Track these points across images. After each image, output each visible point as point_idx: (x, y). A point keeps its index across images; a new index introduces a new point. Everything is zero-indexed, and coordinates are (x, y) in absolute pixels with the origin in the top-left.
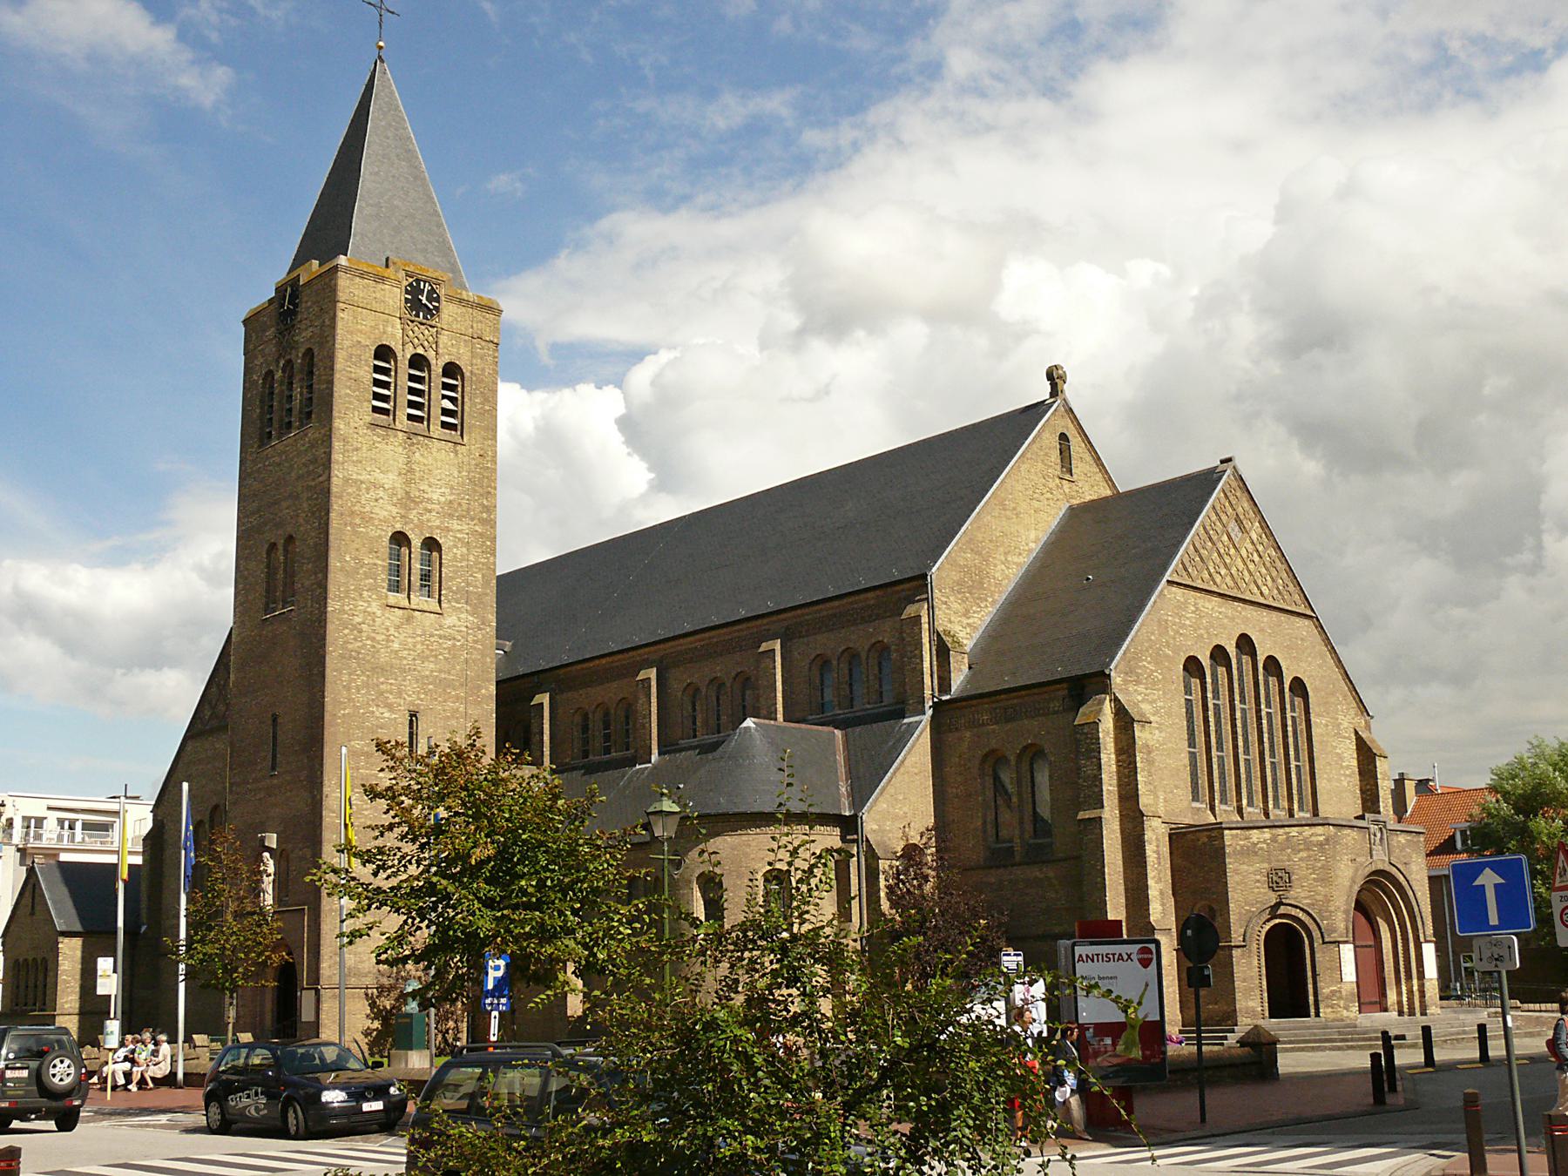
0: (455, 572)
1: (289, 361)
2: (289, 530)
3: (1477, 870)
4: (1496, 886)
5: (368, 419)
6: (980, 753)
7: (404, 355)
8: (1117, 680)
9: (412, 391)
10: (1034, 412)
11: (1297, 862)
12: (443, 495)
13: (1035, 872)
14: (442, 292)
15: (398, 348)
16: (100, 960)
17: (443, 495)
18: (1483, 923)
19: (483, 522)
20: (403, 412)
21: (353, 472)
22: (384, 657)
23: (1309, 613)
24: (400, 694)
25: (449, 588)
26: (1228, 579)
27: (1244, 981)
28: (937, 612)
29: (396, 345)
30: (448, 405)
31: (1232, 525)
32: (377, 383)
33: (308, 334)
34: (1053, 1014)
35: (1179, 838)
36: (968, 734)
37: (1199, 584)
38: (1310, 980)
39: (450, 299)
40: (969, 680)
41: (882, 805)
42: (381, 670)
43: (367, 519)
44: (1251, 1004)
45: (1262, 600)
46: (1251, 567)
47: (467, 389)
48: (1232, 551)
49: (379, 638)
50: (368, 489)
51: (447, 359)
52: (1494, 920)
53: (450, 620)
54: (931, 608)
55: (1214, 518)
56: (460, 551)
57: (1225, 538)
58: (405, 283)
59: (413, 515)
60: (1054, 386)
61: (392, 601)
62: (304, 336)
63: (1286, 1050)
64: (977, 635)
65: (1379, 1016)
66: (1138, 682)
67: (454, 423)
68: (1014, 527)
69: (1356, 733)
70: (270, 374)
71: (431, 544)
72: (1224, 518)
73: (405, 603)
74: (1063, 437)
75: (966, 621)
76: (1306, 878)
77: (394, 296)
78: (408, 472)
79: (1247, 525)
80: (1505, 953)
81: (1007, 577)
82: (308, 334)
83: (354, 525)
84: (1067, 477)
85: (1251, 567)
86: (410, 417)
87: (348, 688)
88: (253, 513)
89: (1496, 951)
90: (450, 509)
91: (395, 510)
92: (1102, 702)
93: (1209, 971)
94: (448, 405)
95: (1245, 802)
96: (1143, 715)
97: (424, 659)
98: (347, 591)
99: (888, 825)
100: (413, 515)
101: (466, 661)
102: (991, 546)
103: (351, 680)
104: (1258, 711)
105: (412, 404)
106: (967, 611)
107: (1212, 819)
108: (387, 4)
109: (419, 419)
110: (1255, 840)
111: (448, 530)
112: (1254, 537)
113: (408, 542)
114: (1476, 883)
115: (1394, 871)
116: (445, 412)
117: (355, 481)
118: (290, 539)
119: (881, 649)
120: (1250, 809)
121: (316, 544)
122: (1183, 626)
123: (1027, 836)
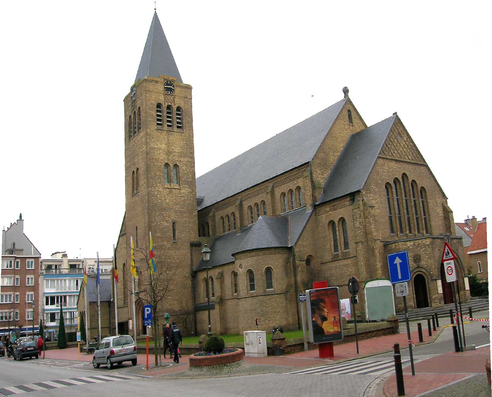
1: (135, 112)
2: (137, 166)
6: (328, 221)
7: (165, 106)
11: (422, 252)
13: (345, 262)
20: (166, 124)
32: (158, 115)
34: (353, 309)
37: (388, 157)
38: (428, 293)
44: (411, 303)
45: (409, 161)
46: (405, 150)
51: (177, 105)
52: (400, 277)
53: (183, 191)
55: (392, 134)
56: (184, 168)
57: (396, 140)
61: (166, 186)
63: (401, 322)
66: (371, 193)
69: (443, 204)
70: (130, 116)
71: (176, 166)
73: (169, 187)
74: (349, 111)
75: (322, 177)
76: (425, 258)
77: (161, 87)
78: (168, 144)
81: (334, 160)
83: (153, 162)
84: (351, 124)
85: (405, 150)
86: (168, 126)
87: (154, 216)
90: (181, 155)
93: (357, 298)
95: (408, 232)
102: (329, 150)
103: (155, 214)
105: (168, 121)
109: (160, 124)
110: (408, 245)
113: (399, 181)
116: (178, 123)
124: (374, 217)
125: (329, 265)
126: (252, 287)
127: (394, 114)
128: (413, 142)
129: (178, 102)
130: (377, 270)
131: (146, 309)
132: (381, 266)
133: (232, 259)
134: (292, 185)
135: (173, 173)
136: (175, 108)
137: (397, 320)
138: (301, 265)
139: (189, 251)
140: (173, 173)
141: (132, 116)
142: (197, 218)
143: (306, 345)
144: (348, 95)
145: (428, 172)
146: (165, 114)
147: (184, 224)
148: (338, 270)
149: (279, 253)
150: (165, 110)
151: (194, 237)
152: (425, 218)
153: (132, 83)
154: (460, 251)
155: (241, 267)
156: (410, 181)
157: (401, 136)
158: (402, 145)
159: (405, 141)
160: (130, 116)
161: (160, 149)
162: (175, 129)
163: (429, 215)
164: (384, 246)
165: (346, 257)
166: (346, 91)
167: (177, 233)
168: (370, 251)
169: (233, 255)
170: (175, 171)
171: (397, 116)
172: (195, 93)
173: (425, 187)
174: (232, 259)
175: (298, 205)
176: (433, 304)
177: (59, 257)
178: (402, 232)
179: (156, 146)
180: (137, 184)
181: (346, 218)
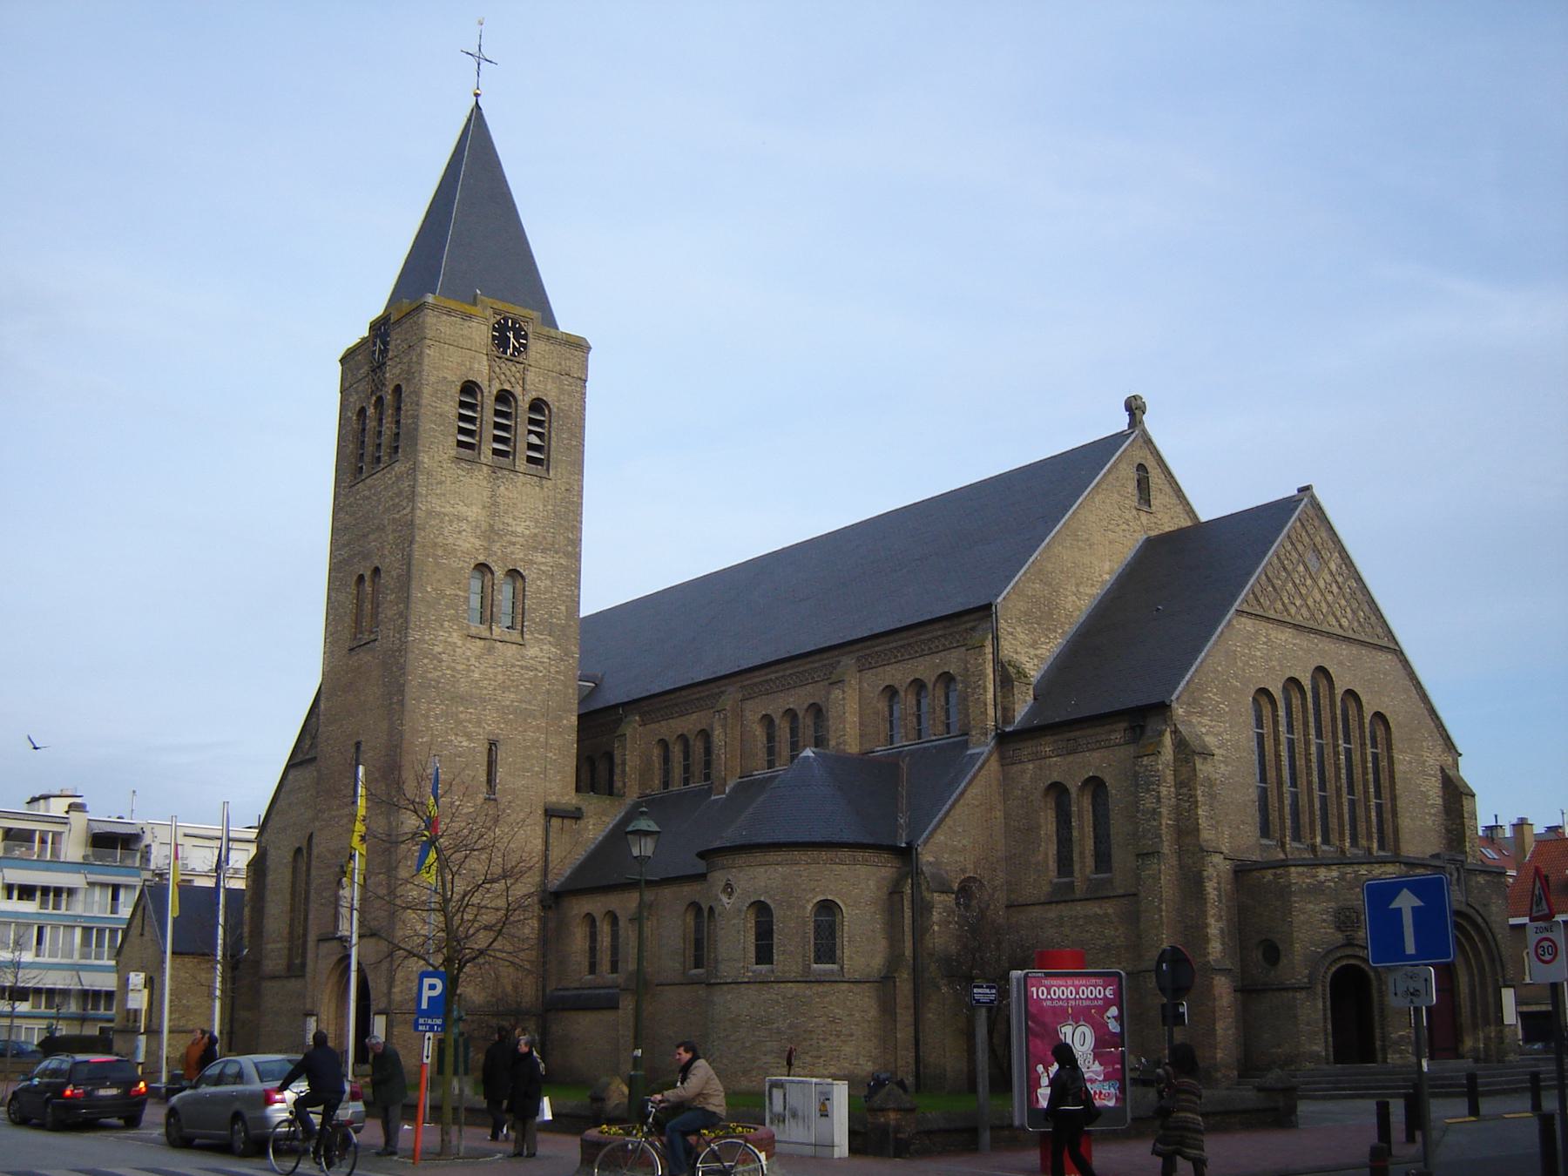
0: (539, 604)
2: (377, 563)
3: (1393, 889)
4: (1413, 908)
5: (453, 453)
7: (490, 390)
8: (1179, 711)
9: (497, 426)
10: (1110, 444)
12: (527, 528)
13: (1094, 909)
14: (530, 329)
15: (484, 384)
16: (132, 975)
17: (527, 528)
18: (1398, 953)
19: (567, 555)
20: (488, 447)
21: (437, 504)
22: (463, 687)
23: (1385, 642)
24: (479, 723)
25: (532, 620)
26: (1304, 611)
27: (1308, 1024)
28: (1002, 642)
29: (483, 381)
30: (534, 440)
31: (1309, 556)
32: (462, 418)
33: (397, 371)
35: (1242, 871)
36: (1031, 766)
37: (1271, 614)
38: (1377, 1025)
39: (539, 336)
40: (1033, 712)
41: (940, 837)
42: (463, 699)
43: (450, 551)
44: (1315, 1048)
45: (1340, 632)
46: (1330, 598)
47: (554, 425)
48: (1309, 582)
49: (459, 667)
50: (451, 522)
51: (534, 395)
52: (1410, 948)
53: (532, 651)
54: (996, 638)
55: (1289, 547)
57: (1301, 568)
58: (493, 321)
59: (496, 547)
60: (1132, 415)
61: (473, 631)
62: (392, 374)
64: (1044, 667)
65: (1452, 1063)
66: (1202, 714)
67: (539, 459)
68: (1090, 555)
69: (1442, 770)
70: (362, 411)
72: (1300, 547)
73: (486, 634)
74: (1141, 467)
75: (1032, 652)
77: (480, 332)
78: (493, 506)
79: (1326, 555)
80: (1420, 986)
82: (397, 371)
83: (435, 557)
84: (1145, 508)
85: (1330, 598)
87: (427, 717)
88: (344, 546)
89: (1412, 985)
90: (535, 544)
91: (478, 543)
92: (1161, 733)
93: (1184, 1009)
94: (534, 440)
95: (1319, 840)
96: (1205, 746)
97: (505, 689)
98: (428, 622)
99: (946, 857)
100: (496, 547)
101: (548, 692)
103: (430, 710)
104: (1336, 746)
105: (497, 439)
106: (1035, 642)
107: (1282, 856)
108: (486, 53)
110: (1322, 878)
111: (532, 562)
112: (1333, 567)
114: (1394, 905)
115: (1471, 912)
116: (531, 447)
117: (438, 514)
118: (377, 571)
119: (947, 679)
120: (1325, 848)
121: (399, 576)
122: (1254, 658)
123: (1088, 871)
124: (1211, 786)
125: (1036, 912)
126: (764, 954)
127: (1300, 490)
128: (1359, 579)
129: (534, 382)
130: (1206, 939)
131: (427, 982)
132: (1222, 931)
133: (701, 866)
134: (925, 668)
135: (504, 594)
136: (524, 402)
137: (1294, 1089)
138: (941, 903)
139: (539, 831)
140: (504, 594)
141: (371, 411)
142: (574, 736)
143: (986, 1137)
144: (1141, 422)
145: (1403, 673)
146: (489, 417)
147: (527, 748)
148: (1067, 931)
149: (865, 862)
150: (490, 404)
151: (562, 790)
152: (1379, 807)
153: (378, 310)
154: (1494, 909)
155: (729, 889)
156: (1339, 692)
157: (1319, 556)
158: (1322, 584)
159: (1331, 573)
160: (362, 411)
161: (460, 518)
162: (521, 465)
163: (1394, 798)
164: (1236, 872)
165: (1096, 894)
166: (1134, 408)
167: (501, 772)
168: (1192, 884)
169: (702, 855)
170: (507, 590)
171: (1313, 497)
172: (596, 364)
173: (1388, 716)
174: (701, 866)
175: (941, 728)
176: (1393, 1058)
177: (58, 807)
178: (1297, 837)
179: (448, 509)
180: (375, 614)
181: (1108, 781)
